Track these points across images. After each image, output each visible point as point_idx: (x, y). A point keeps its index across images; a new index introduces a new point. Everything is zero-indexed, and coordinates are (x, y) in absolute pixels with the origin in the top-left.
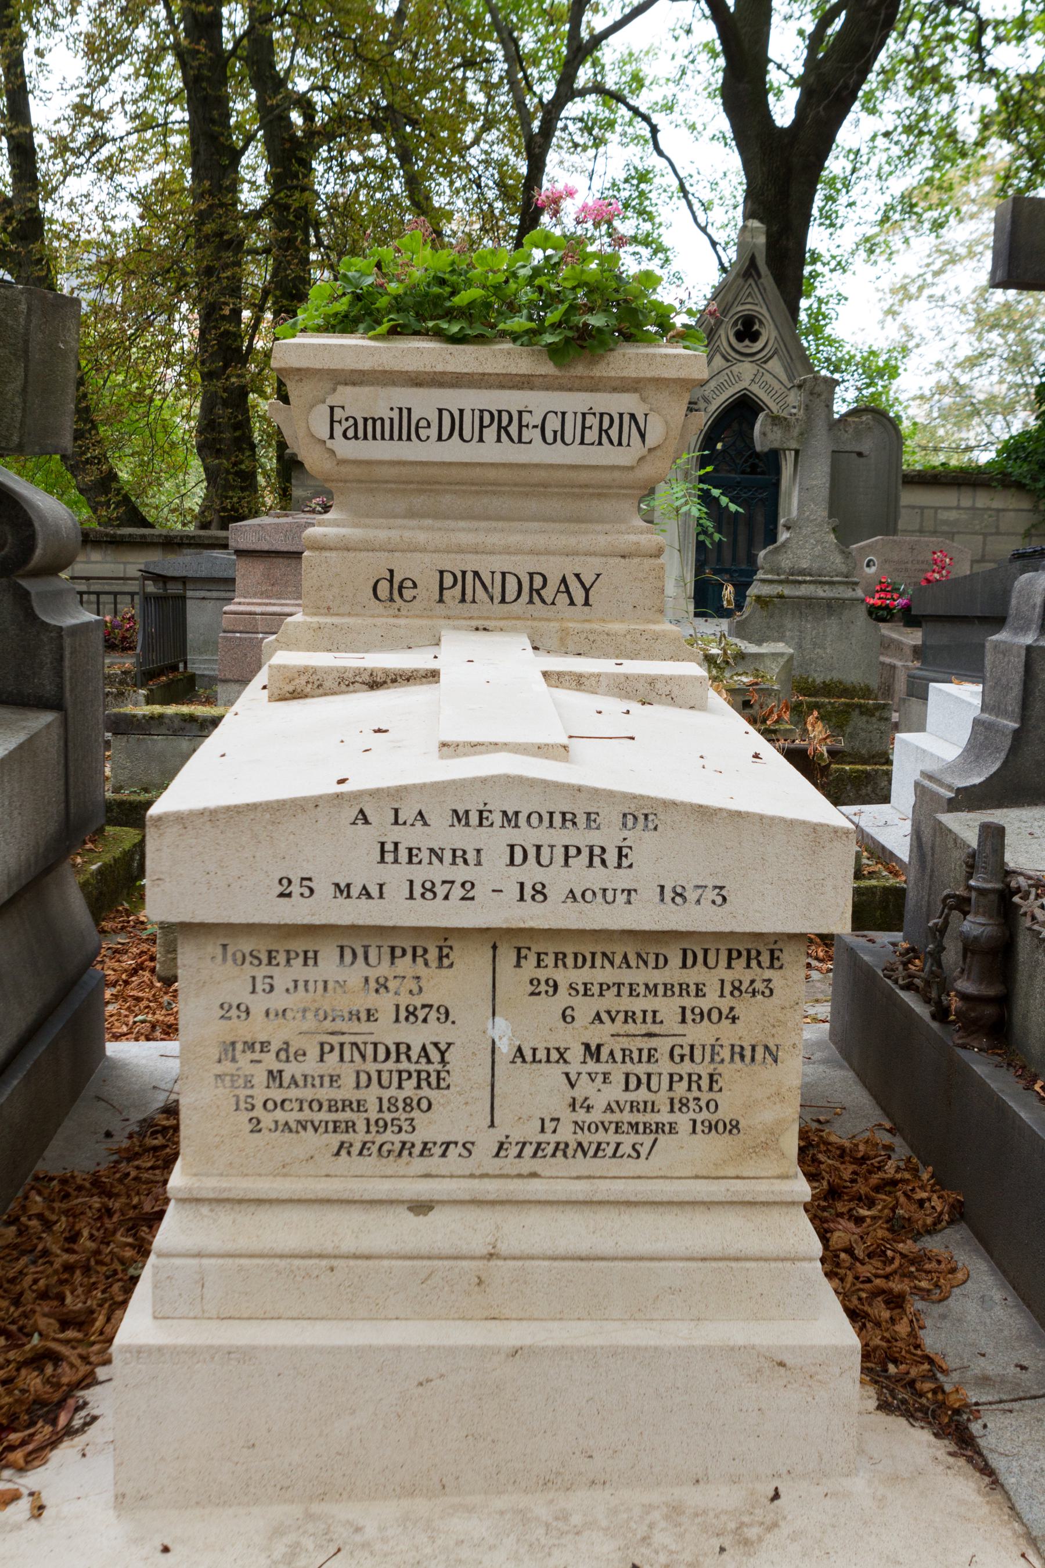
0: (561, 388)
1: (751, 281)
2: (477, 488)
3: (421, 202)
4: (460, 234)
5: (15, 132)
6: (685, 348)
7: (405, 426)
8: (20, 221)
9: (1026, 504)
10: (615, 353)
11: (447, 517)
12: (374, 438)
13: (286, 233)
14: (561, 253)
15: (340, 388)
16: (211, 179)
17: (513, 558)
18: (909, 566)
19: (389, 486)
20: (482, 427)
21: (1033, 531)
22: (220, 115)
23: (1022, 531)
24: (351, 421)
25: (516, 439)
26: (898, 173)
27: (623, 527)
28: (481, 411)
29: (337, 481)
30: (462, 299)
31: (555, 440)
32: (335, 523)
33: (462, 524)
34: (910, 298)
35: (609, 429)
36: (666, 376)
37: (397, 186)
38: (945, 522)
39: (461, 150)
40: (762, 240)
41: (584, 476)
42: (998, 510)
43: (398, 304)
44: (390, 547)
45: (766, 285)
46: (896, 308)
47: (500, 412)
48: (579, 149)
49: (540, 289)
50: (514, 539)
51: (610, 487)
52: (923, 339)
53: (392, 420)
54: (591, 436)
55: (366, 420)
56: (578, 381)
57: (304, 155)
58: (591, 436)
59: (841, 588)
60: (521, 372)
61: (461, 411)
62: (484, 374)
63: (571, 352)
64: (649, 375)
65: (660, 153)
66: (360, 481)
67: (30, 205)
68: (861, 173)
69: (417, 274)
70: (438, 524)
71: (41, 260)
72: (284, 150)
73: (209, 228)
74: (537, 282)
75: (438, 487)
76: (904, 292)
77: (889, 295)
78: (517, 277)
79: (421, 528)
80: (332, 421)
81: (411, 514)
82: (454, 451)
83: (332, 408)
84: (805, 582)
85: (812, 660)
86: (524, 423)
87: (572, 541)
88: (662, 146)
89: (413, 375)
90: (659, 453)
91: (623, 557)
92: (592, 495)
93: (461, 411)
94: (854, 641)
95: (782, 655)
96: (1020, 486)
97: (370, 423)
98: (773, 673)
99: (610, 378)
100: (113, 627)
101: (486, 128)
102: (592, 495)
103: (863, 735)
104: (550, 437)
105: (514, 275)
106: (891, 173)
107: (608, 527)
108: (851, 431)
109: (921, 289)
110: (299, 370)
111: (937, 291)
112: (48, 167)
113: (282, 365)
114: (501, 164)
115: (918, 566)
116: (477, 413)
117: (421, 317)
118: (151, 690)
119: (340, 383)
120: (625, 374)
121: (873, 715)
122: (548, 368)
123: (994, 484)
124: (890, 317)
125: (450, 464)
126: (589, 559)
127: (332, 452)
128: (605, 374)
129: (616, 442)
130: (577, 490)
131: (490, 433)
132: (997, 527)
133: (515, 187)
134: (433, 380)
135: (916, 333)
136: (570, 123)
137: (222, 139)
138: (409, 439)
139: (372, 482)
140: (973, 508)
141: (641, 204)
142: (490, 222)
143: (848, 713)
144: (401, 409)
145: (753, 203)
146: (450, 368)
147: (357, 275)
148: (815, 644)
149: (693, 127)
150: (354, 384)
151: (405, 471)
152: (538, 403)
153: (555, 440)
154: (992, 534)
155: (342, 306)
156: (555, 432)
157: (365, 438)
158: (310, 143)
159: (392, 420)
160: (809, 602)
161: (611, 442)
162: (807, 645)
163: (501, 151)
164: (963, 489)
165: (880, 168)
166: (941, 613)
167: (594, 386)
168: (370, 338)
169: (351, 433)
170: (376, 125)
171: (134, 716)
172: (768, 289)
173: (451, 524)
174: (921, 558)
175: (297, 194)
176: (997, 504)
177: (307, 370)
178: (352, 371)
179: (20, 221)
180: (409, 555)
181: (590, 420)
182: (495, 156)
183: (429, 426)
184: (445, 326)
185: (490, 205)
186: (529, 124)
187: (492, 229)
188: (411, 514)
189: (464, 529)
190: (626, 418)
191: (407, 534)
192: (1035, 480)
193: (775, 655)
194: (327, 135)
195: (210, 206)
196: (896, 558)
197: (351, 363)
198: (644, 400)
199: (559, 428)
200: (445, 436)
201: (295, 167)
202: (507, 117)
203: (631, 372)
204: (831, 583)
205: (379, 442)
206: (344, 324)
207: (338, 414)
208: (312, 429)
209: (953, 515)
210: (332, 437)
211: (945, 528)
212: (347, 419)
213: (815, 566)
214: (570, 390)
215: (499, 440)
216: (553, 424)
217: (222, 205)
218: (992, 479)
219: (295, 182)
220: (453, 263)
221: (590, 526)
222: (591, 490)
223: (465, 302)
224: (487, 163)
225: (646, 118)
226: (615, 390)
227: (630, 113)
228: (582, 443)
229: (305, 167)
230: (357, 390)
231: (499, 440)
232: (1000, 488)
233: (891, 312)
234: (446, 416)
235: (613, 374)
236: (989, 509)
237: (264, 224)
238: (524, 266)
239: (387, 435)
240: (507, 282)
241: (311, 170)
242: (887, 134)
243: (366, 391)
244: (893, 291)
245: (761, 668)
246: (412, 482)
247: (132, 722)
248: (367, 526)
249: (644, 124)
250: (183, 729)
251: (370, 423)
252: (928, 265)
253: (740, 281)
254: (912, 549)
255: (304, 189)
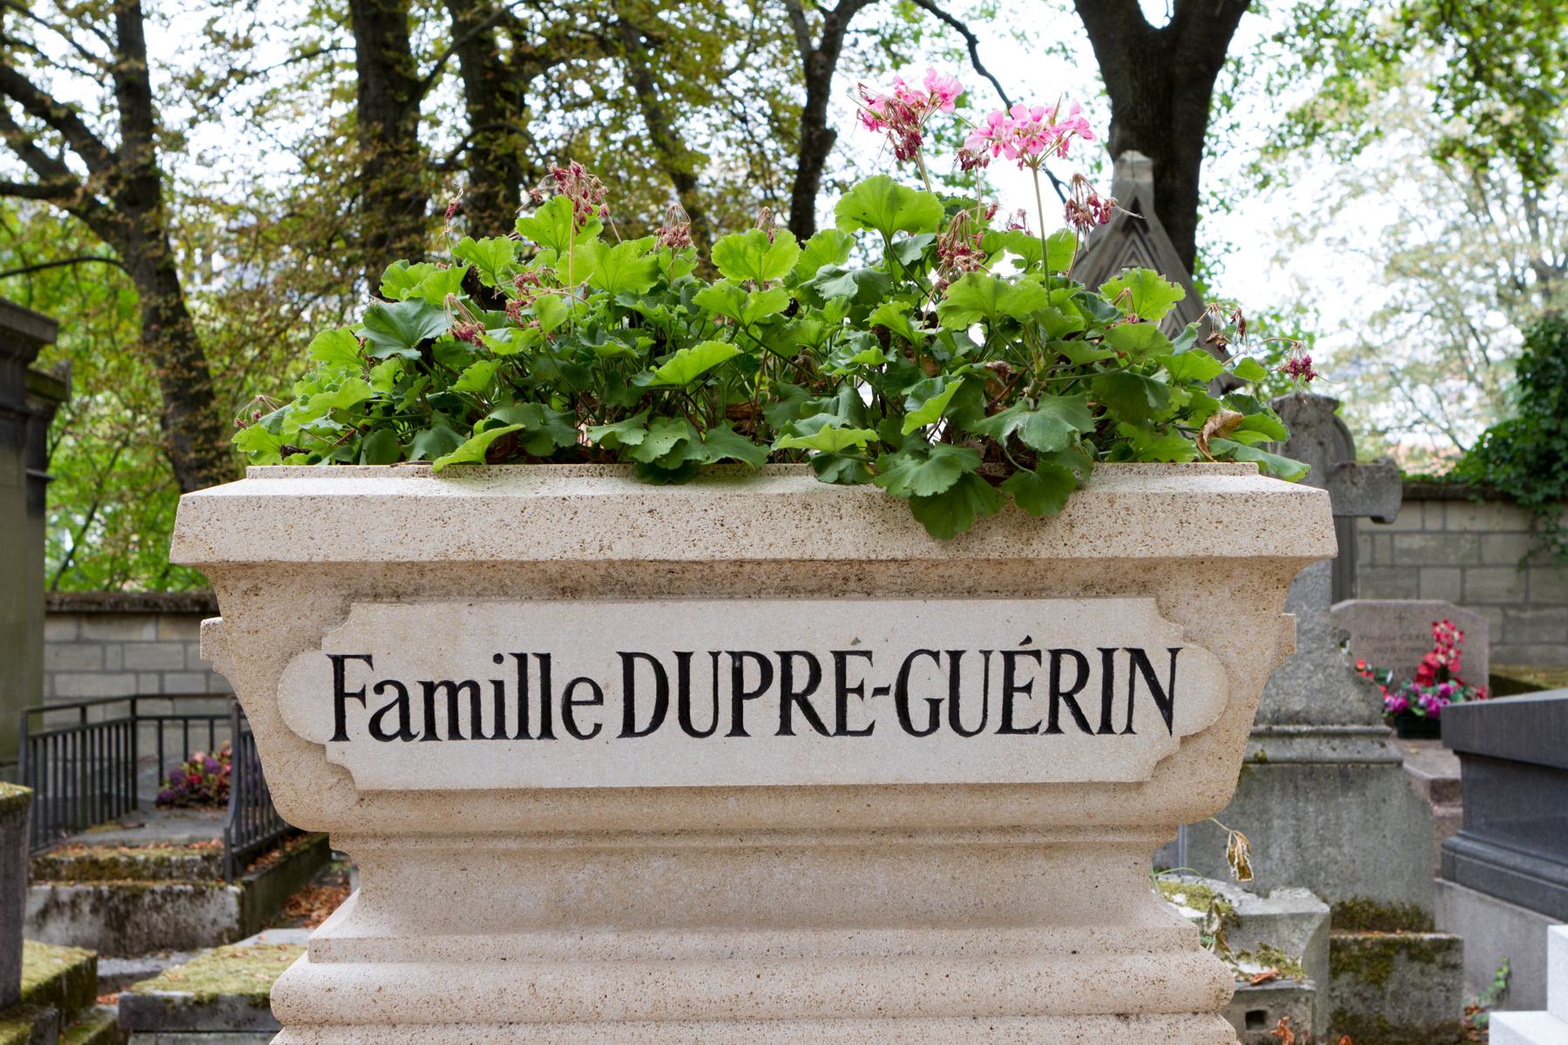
0: (948, 589)
1: (1134, 236)
2: (731, 842)
3: (665, 141)
4: (721, 183)
5: (124, 67)
6: (1264, 471)
7: (536, 702)
8: (129, 182)
9: (1515, 522)
10: (1088, 496)
11: (654, 922)
12: (454, 733)
13: (483, 188)
14: (926, 239)
15: (359, 610)
16: (383, 120)
17: (831, 1032)
18: (1397, 643)
19: (502, 845)
20: (739, 696)
21: (1531, 561)
22: (396, 38)
23: (1515, 560)
24: (391, 694)
25: (831, 726)
26: (1292, 84)
27: (1118, 934)
28: (737, 656)
29: (364, 837)
30: (681, 366)
31: (934, 724)
32: (359, 951)
33: (694, 941)
34: (1302, 242)
35: (1076, 691)
36: (1226, 551)
37: (637, 124)
38: (1407, 552)
39: (719, 77)
40: (1147, 179)
41: (1011, 809)
42: (1480, 534)
43: (519, 381)
44: (504, 1013)
45: (1156, 241)
46: (1282, 255)
47: (786, 657)
48: (875, 71)
49: (884, 336)
50: (833, 982)
51: (1078, 829)
52: (1320, 293)
53: (499, 686)
54: (1030, 709)
55: (429, 688)
56: (990, 572)
57: (511, 87)
58: (1030, 709)
59: (1361, 743)
60: (840, 554)
61: (684, 659)
62: (741, 563)
63: (975, 505)
64: (1179, 550)
65: (981, 70)
66: (426, 836)
67: (142, 161)
68: (1243, 87)
69: (561, 305)
70: (629, 943)
71: (157, 232)
72: (485, 82)
73: (377, 185)
74: (874, 318)
75: (627, 843)
76: (1294, 234)
77: (1274, 237)
78: (821, 303)
79: (585, 957)
80: (340, 696)
81: (563, 916)
82: (666, 758)
83: (338, 662)
84: (1300, 734)
85: (1320, 867)
86: (851, 683)
87: (985, 982)
88: (982, 62)
89: (553, 570)
90: (1207, 744)
91: (1123, 1016)
92: (1030, 848)
93: (684, 659)
94: (1388, 833)
95: (1309, 916)
96: (1508, 499)
97: (441, 696)
98: (1298, 948)
99: (1075, 561)
100: (207, 770)
101: (752, 49)
102: (1030, 848)
103: (1416, 995)
104: (920, 718)
105: (815, 296)
106: (1283, 86)
107: (1075, 936)
108: (1362, 481)
109: (1314, 230)
110: (247, 566)
111: (1336, 231)
112: (172, 116)
113: (202, 556)
114: (772, 95)
115: (1410, 644)
116: (726, 663)
117: (578, 405)
118: (248, 885)
119: (356, 595)
120: (1117, 550)
121: (1430, 961)
122: (917, 545)
123: (1472, 497)
124: (1276, 265)
125: (658, 791)
126: (1033, 1027)
127: (344, 773)
128: (1064, 553)
129: (1095, 724)
130: (990, 840)
131: (763, 712)
132: (1480, 557)
133: (792, 122)
134: (606, 579)
135: (1310, 284)
136: (862, 37)
137: (399, 69)
138: (547, 732)
139: (455, 836)
140: (1444, 532)
141: (957, 135)
142: (760, 168)
143: (1389, 958)
144: (522, 659)
145: (1123, 129)
146: (651, 550)
147: (413, 309)
148: (1323, 839)
149: (1021, 37)
150: (397, 596)
151: (539, 814)
152: (887, 629)
153: (934, 724)
154: (1472, 567)
155: (378, 385)
156: (934, 704)
157: (431, 733)
158: (520, 71)
159: (499, 686)
160: (1310, 770)
161: (1083, 724)
162: (1310, 840)
163: (768, 78)
164: (1428, 505)
165: (1271, 79)
166: (1500, 752)
167: (1032, 584)
168: (441, 474)
169: (390, 723)
170: (604, 46)
171: (168, 1000)
172: (1160, 247)
173: (664, 941)
174: (1413, 631)
175: (502, 140)
176: (1480, 524)
177: (269, 566)
178: (389, 565)
179: (129, 182)
180: (554, 1033)
181: (1025, 670)
182: (764, 84)
183: (599, 698)
184: (634, 439)
185: (760, 145)
186: (809, 42)
187: (763, 175)
188: (562, 916)
189: (699, 957)
190: (1122, 662)
191: (550, 978)
192: (1529, 489)
193: (1297, 918)
194: (543, 61)
195: (382, 155)
196: (1377, 632)
197: (383, 545)
198: (1165, 612)
199: (943, 692)
200: (642, 723)
201: (500, 102)
202: (780, 35)
203: (1131, 545)
204: (1344, 735)
205: (468, 745)
206: (374, 436)
207: (356, 675)
208: (288, 718)
209: (1416, 542)
210: (341, 734)
211: (1407, 560)
212: (379, 689)
213: (1316, 706)
214: (971, 592)
215: (785, 728)
216: (928, 682)
217: (396, 153)
218: (1469, 490)
219: (500, 121)
220: (656, 271)
221: (1032, 936)
222: (1028, 839)
223: (690, 374)
224: (754, 92)
225: (960, 28)
226: (1088, 589)
227: (941, 21)
228: (1007, 727)
229: (513, 102)
230: (403, 611)
231: (785, 728)
232: (1481, 502)
233: (1280, 259)
234: (643, 670)
235: (1084, 551)
236: (1465, 532)
237: (461, 179)
238: (838, 274)
239: (488, 726)
240: (793, 310)
241: (522, 106)
242: (1280, 38)
243: (427, 614)
244: (1280, 234)
245: (1273, 943)
246: (561, 834)
247: (164, 1012)
248: (442, 956)
249: (960, 35)
250: (251, 1021)
251: (441, 696)
252: (1321, 201)
253: (1119, 237)
254: (1401, 618)
255: (511, 131)
